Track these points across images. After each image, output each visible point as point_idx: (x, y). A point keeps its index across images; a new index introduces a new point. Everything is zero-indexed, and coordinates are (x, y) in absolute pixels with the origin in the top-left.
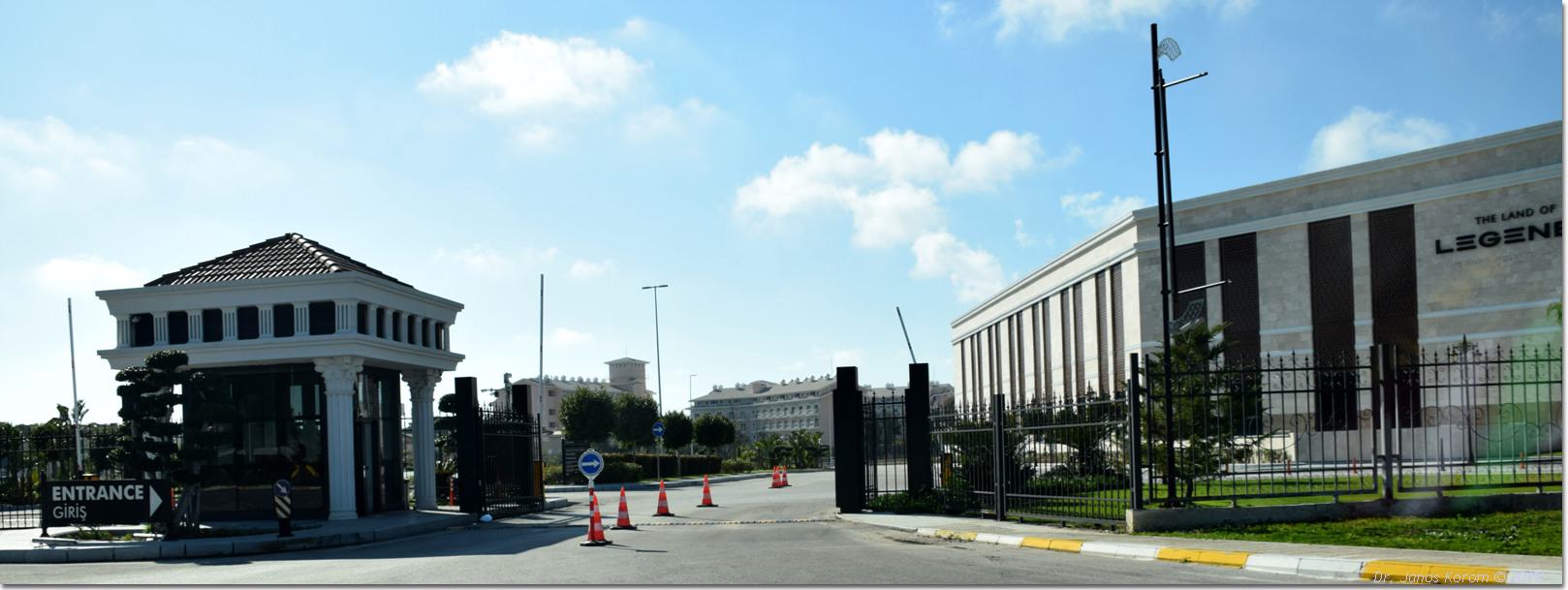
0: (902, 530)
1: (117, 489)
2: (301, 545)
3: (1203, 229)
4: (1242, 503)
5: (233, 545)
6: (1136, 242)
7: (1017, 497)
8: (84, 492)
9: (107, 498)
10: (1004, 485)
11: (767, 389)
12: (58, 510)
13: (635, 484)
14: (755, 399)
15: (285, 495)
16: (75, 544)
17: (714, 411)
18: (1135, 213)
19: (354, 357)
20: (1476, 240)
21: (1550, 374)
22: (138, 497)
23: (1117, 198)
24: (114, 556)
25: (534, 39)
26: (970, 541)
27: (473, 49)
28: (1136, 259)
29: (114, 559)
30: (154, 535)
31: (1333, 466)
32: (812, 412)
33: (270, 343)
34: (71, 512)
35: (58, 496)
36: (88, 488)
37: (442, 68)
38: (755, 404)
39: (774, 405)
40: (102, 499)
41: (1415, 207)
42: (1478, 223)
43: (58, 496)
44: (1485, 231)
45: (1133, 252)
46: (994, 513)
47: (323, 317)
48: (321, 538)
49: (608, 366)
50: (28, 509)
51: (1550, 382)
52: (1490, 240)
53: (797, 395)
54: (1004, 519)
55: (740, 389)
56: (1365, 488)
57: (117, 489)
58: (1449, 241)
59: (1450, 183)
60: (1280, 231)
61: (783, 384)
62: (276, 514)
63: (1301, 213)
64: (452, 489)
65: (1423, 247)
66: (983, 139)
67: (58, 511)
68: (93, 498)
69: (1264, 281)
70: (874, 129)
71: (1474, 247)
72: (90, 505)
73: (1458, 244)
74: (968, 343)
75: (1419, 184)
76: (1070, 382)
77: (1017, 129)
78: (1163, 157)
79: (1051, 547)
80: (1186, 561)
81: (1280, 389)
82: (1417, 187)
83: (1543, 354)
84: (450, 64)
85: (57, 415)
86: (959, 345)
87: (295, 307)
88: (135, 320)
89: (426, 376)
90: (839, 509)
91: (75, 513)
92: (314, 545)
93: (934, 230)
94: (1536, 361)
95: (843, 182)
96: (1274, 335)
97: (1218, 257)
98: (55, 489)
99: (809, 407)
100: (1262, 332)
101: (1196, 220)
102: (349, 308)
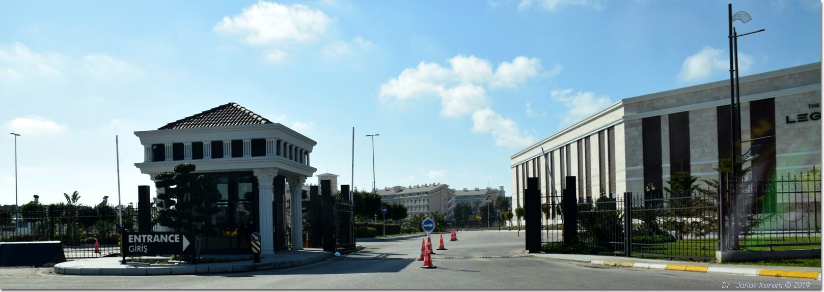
0: (581, 262)
1: (165, 237)
2: (266, 267)
3: (660, 109)
4: (775, 249)
5: (233, 266)
6: (623, 115)
7: (620, 244)
8: (146, 238)
9: (159, 241)
10: (631, 239)
11: (402, 191)
12: (132, 248)
13: (373, 239)
14: (395, 196)
15: (257, 240)
16: (149, 266)
17: (465, 200)
18: (623, 100)
19: (275, 168)
20: (808, 117)
21: (815, 185)
22: (176, 241)
23: (580, 92)
24: (171, 272)
25: (276, 5)
26: (629, 267)
27: (243, 9)
28: (623, 124)
29: (171, 274)
30: (179, 261)
31: (775, 232)
32: (426, 203)
33: (231, 161)
34: (139, 248)
35: (131, 240)
36: (148, 236)
37: (227, 19)
38: (395, 198)
39: (422, 197)
40: (156, 242)
41: (775, 99)
42: (810, 107)
43: (131, 240)
44: (813, 112)
45: (622, 120)
46: (624, 253)
47: (259, 147)
48: (276, 263)
49: (317, 177)
50: (115, 247)
51: (789, 193)
52: (816, 116)
53: (418, 194)
54: (630, 256)
55: (387, 190)
56: (798, 243)
57: (165, 237)
58: (793, 117)
59: (794, 87)
60: (702, 111)
61: (410, 188)
62: (252, 251)
63: (713, 102)
64: (307, 239)
65: (779, 119)
66: (510, 60)
67: (131, 248)
68: (151, 241)
69: (693, 137)
70: (453, 55)
71: (807, 120)
72: (149, 245)
73: (798, 118)
74: (520, 168)
75: (778, 87)
76: (583, 188)
77: (528, 54)
78: (734, 72)
79: (687, 269)
80: (778, 276)
81: (781, 191)
82: (777, 89)
83: (786, 179)
84: (231, 17)
85: (33, 199)
86: (515, 168)
87: (204, 143)
88: (154, 147)
89: (299, 179)
90: (528, 251)
91: (141, 249)
92: (272, 267)
93: (484, 108)
94: (782, 182)
95: (436, 82)
96: (698, 165)
97: (668, 124)
98: (130, 236)
99: (424, 200)
100: (691, 163)
101: (656, 104)
102: (273, 142)
